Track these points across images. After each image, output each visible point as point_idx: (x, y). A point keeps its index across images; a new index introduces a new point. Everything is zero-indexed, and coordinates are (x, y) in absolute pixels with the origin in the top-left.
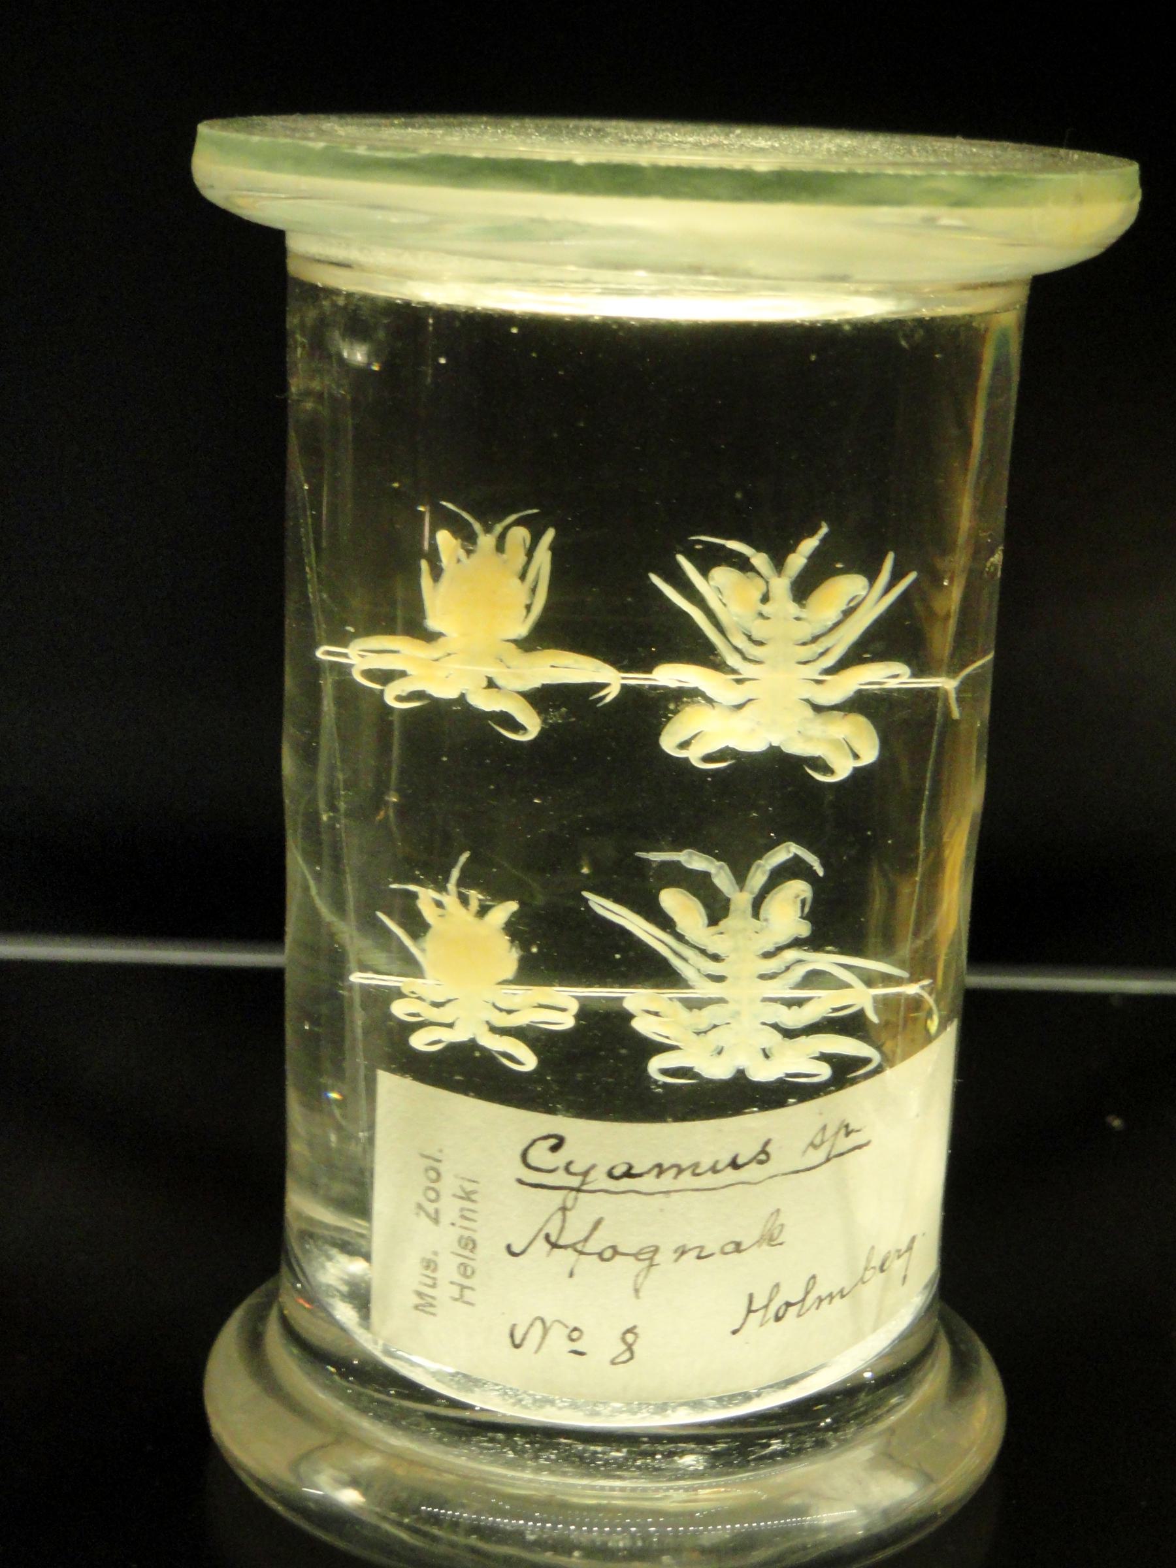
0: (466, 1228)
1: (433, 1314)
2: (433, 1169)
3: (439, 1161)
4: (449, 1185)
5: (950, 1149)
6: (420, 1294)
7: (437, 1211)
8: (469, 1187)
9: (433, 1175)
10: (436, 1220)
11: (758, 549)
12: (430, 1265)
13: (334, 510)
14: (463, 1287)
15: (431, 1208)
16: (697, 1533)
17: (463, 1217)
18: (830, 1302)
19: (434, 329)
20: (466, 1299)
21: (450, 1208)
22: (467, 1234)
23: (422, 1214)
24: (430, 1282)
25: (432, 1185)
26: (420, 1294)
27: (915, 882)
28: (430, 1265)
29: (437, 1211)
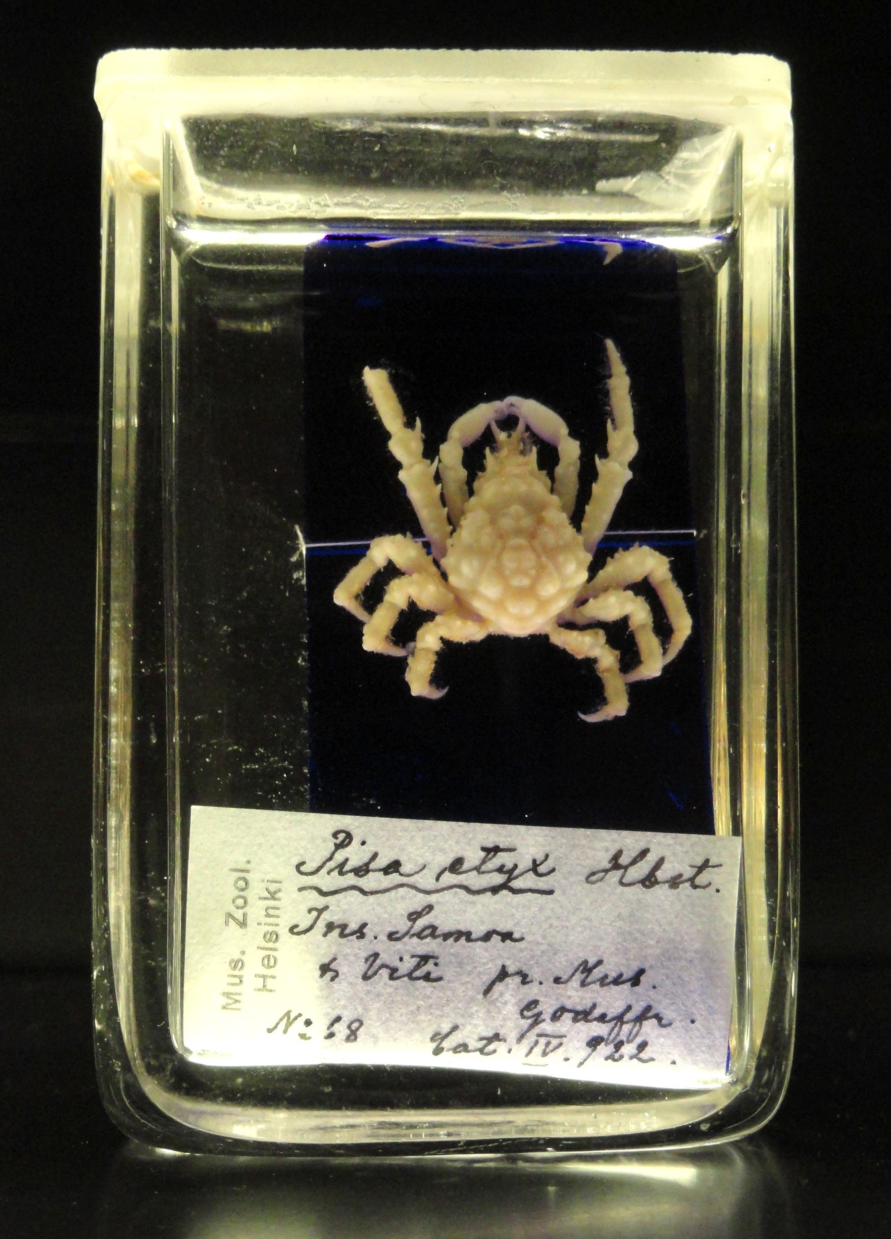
0: (271, 949)
1: (239, 1009)
2: (239, 897)
3: (247, 871)
4: (256, 890)
5: (384, 590)
6: (227, 995)
7: (245, 915)
8: (273, 887)
9: (242, 884)
10: (243, 924)
11: (640, 432)
12: (237, 964)
13: (783, 646)
14: (264, 977)
15: (239, 914)
16: (423, 963)
17: (268, 915)
18: (621, 975)
19: (276, 768)
20: (268, 988)
21: (256, 910)
22: (270, 929)
23: (231, 922)
24: (271, 912)
25: (242, 893)
26: (227, 995)
27: (762, 689)
28: (237, 964)
29: (245, 915)
